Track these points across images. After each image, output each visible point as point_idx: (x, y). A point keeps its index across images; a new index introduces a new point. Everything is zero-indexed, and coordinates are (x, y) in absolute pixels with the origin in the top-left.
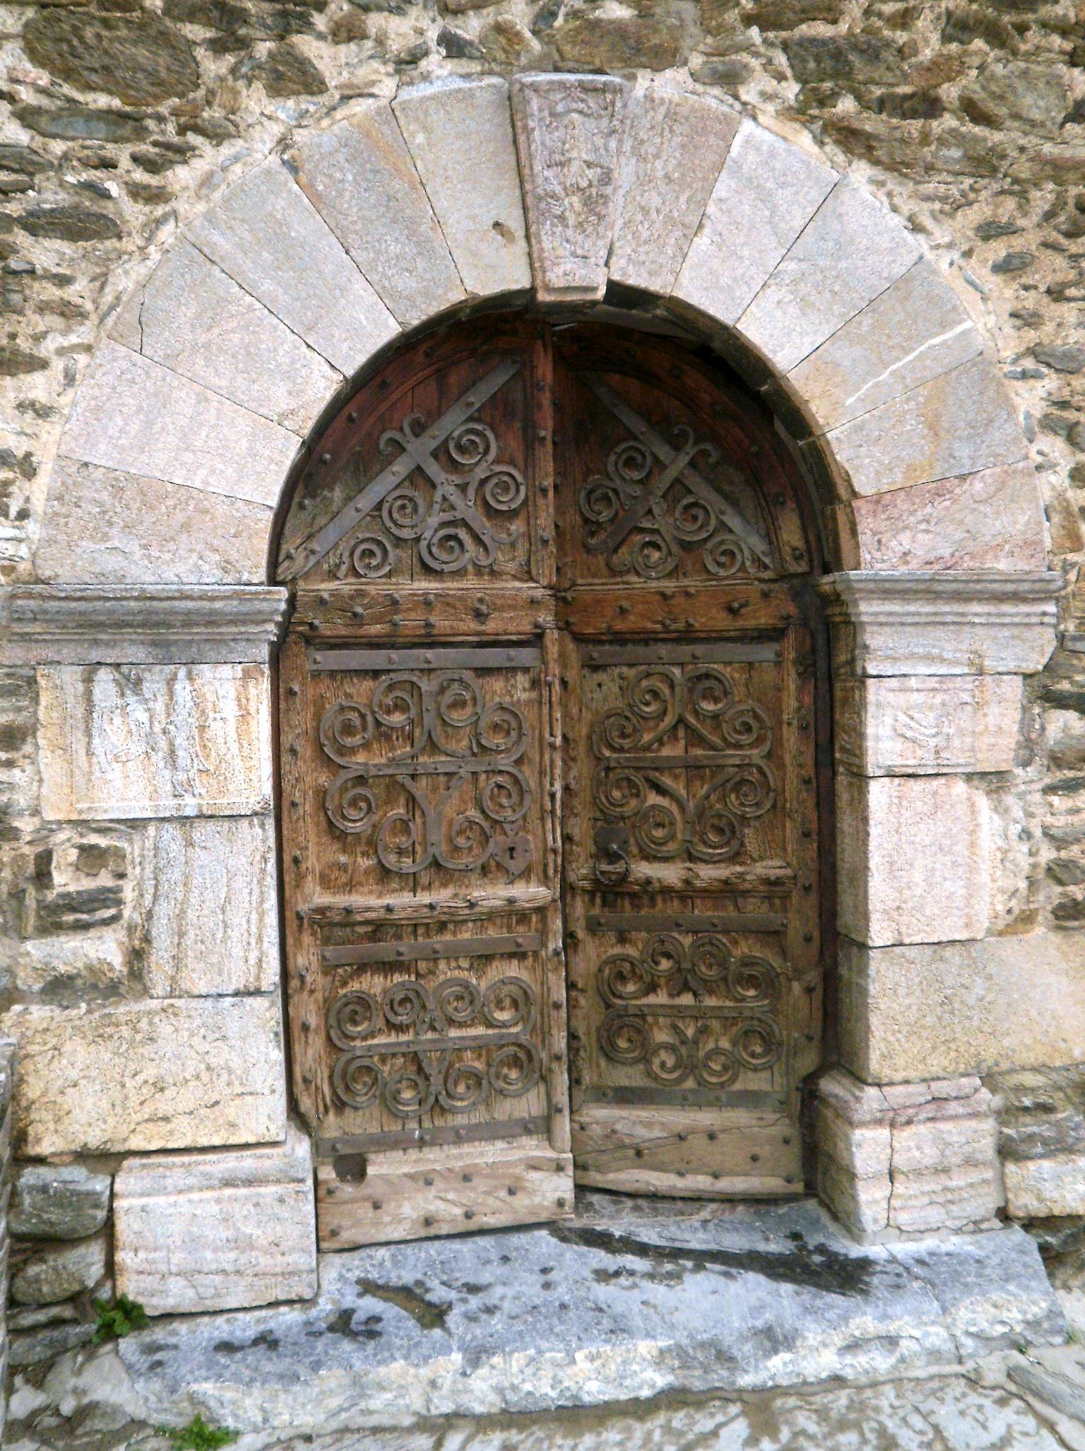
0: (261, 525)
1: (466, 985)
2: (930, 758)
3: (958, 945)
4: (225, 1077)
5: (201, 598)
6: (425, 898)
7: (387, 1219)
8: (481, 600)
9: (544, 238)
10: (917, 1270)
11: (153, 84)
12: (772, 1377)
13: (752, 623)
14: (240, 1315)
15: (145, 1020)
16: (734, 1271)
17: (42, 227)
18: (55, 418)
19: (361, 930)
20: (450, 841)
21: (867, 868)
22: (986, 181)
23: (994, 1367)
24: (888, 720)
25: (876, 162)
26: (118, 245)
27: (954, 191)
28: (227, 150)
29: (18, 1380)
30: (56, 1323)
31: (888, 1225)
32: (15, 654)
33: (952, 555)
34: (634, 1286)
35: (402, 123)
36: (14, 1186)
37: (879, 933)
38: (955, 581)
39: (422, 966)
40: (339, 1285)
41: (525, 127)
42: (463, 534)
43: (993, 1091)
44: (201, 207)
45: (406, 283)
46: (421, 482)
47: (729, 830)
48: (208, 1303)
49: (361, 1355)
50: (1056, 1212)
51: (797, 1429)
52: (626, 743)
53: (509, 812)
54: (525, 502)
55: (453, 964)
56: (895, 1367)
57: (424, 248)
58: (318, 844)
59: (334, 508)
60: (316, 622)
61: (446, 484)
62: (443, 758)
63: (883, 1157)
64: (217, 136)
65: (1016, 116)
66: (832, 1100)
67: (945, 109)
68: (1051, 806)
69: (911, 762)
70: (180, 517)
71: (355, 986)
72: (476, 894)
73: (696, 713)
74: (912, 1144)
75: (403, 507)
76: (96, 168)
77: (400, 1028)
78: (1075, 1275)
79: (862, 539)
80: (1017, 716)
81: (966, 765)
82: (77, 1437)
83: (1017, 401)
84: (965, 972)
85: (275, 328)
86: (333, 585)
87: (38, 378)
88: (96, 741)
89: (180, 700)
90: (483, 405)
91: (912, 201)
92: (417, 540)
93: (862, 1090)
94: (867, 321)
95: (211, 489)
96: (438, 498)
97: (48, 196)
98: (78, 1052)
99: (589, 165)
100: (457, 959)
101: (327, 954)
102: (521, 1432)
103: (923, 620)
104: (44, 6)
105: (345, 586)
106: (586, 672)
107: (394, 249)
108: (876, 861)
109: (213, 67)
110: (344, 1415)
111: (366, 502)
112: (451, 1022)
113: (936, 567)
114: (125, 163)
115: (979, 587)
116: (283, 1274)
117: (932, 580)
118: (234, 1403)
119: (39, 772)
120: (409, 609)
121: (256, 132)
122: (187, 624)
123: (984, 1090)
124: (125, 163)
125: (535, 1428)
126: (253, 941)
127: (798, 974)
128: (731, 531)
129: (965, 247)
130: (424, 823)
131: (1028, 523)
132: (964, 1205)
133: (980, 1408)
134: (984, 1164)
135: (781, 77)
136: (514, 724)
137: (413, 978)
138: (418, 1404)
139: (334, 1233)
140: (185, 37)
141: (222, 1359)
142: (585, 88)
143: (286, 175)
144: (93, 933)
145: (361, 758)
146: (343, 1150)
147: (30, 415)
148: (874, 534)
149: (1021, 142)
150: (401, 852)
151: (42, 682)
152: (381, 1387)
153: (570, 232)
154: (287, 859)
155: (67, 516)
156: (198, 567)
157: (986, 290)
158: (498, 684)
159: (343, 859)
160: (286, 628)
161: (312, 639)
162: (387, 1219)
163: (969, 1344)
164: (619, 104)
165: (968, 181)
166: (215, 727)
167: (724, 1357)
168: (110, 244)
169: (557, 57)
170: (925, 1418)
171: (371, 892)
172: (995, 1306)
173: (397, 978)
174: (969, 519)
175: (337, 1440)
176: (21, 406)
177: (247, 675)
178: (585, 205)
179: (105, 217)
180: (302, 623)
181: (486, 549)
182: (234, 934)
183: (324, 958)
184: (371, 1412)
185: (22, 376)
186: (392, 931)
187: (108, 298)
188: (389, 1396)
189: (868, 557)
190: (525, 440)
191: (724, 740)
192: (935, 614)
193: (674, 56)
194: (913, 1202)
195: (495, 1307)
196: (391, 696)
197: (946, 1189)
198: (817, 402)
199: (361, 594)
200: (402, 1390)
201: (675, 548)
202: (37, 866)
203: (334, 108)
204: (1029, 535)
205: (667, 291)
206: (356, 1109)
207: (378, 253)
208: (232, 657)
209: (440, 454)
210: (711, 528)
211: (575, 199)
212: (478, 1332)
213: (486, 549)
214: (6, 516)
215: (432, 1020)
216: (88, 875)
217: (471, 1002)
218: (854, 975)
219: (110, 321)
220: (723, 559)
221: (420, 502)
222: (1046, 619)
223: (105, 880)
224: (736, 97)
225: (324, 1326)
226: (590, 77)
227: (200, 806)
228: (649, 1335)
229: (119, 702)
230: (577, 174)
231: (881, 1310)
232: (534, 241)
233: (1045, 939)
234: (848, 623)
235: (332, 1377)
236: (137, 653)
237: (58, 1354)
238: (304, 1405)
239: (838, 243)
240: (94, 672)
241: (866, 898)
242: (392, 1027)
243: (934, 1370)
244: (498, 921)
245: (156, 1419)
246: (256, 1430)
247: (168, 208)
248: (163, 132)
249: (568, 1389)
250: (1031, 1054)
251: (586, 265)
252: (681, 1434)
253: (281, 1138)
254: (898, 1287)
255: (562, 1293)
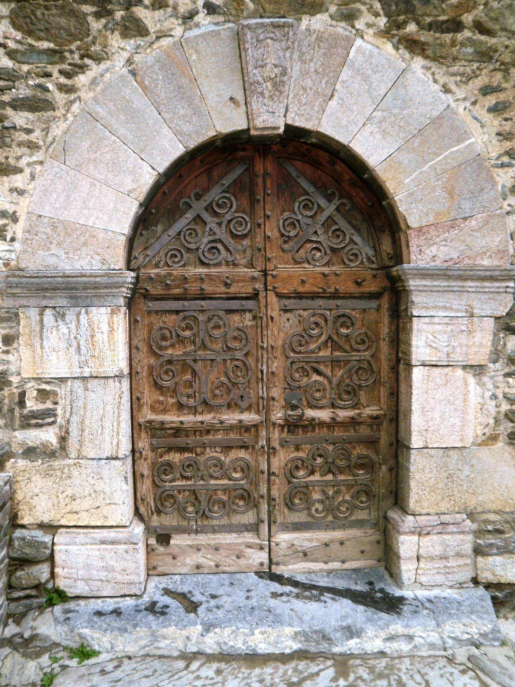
0: (119, 243)
1: (219, 460)
2: (444, 357)
3: (456, 450)
4: (102, 496)
5: (90, 276)
6: (199, 418)
7: (179, 564)
8: (227, 278)
9: (253, 104)
10: (427, 605)
11: (68, 35)
12: (350, 650)
13: (367, 290)
14: (108, 599)
15: (67, 469)
16: (337, 598)
17: (19, 106)
18: (26, 195)
19: (169, 432)
20: (212, 392)
21: (411, 410)
22: (486, 64)
23: (462, 654)
24: (423, 338)
25: (426, 57)
26: (53, 114)
27: (468, 70)
28: (103, 66)
29: (10, 620)
30: (28, 597)
31: (415, 582)
32: (9, 303)
33: (459, 257)
34: (289, 601)
35: (185, 49)
36: (11, 537)
37: (416, 442)
38: (459, 270)
39: (199, 450)
40: (154, 590)
41: (244, 49)
42: (220, 246)
43: (473, 522)
44: (91, 94)
45: (187, 128)
46: (199, 222)
47: (353, 392)
48: (95, 593)
49: (156, 623)
50: (502, 582)
51: (358, 675)
52: (302, 349)
53: (241, 379)
54: (250, 230)
55: (213, 450)
56: (411, 650)
57: (196, 111)
58: (150, 391)
59: (158, 235)
60: (148, 288)
61: (211, 222)
62: (209, 352)
63: (414, 549)
64: (98, 60)
65: (504, 29)
66: (392, 521)
67: (465, 27)
68: (508, 383)
69: (434, 359)
70: (82, 239)
71: (166, 457)
72: (224, 417)
73: (338, 334)
74: (429, 544)
75: (191, 234)
76: (42, 77)
77: (187, 478)
78: (510, 612)
79: (412, 249)
80: (491, 338)
81: (463, 361)
82: (29, 648)
83: (498, 179)
84: (460, 463)
85: (126, 151)
86: (156, 271)
87: (19, 177)
88: (45, 342)
89: (82, 323)
90: (230, 184)
91: (445, 77)
92: (198, 249)
93: (405, 517)
94: (417, 141)
95: (97, 226)
96: (207, 229)
97: (21, 91)
98: (38, 480)
99: (276, 66)
100: (215, 448)
101: (153, 442)
102: (226, 664)
103: (441, 289)
104: (18, 2)
105: (162, 271)
106: (281, 313)
107: (182, 112)
108: (415, 406)
109: (96, 25)
110: (147, 649)
111: (172, 232)
112: (212, 477)
113: (449, 263)
114: (56, 74)
115: (472, 273)
116: (127, 583)
117: (446, 269)
118: (98, 639)
119: (20, 356)
120: (193, 282)
121: (116, 57)
122: (85, 288)
123: (468, 520)
124: (56, 74)
125: (233, 663)
126: (115, 434)
127: (385, 461)
128: (356, 244)
129: (473, 100)
130: (200, 383)
131: (500, 241)
132: (455, 575)
133: (452, 674)
134: (466, 556)
135: (377, 15)
136: (244, 337)
137: (194, 455)
138: (181, 647)
139: (154, 568)
140: (83, 12)
141: (96, 619)
142: (275, 26)
143: (130, 77)
144: (44, 429)
145: (170, 351)
146: (160, 531)
147: (15, 194)
148: (418, 247)
149: (507, 43)
150: (189, 396)
151: (21, 315)
152: (164, 638)
153: (266, 101)
154: (134, 397)
155: (32, 240)
156: (91, 262)
157: (483, 122)
158: (236, 318)
159: (161, 398)
160: (134, 291)
161: (147, 296)
162: (179, 564)
163: (450, 642)
164: (291, 33)
165: (476, 65)
166: (98, 336)
167: (326, 638)
168: (50, 113)
169: (262, 11)
170: (422, 676)
171: (174, 414)
172: (464, 625)
173: (186, 455)
174: (468, 239)
175: (144, 660)
176: (11, 190)
177: (113, 312)
178: (273, 86)
179: (47, 100)
180: (142, 288)
181: (231, 253)
182: (106, 431)
183: (152, 444)
184: (159, 648)
185: (11, 176)
186: (184, 433)
187: (50, 139)
188: (167, 642)
189: (415, 258)
190: (250, 201)
191: (351, 347)
192: (448, 286)
193: (322, 7)
194: (429, 572)
195: (222, 606)
196: (184, 322)
197: (446, 567)
198: (390, 181)
199: (170, 275)
200: (174, 640)
201: (328, 252)
202: (19, 398)
203: (153, 43)
204: (500, 248)
205: (315, 128)
206: (166, 514)
207: (175, 114)
208: (105, 303)
209: (209, 208)
210: (347, 242)
211: (268, 84)
212: (211, 617)
213: (231, 253)
214: (5, 240)
215: (202, 476)
216: (41, 402)
217: (221, 468)
218: (404, 461)
219: (51, 150)
220: (352, 258)
221: (199, 232)
222: (508, 290)
223: (49, 405)
224: (353, 27)
225: (143, 607)
226: (277, 20)
227: (91, 372)
228: (290, 625)
229: (55, 324)
230: (270, 71)
231: (406, 622)
232: (249, 106)
233: (503, 448)
234: (405, 290)
235: (142, 631)
236: (63, 302)
237: (28, 611)
238: (129, 642)
239: (404, 101)
240: (44, 310)
241: (410, 424)
242: (183, 477)
243: (432, 653)
244: (235, 430)
245: (64, 643)
246: (108, 652)
247: (76, 95)
248: (73, 59)
249: (251, 646)
250: (494, 505)
251: (273, 117)
252: (301, 672)
253: (128, 524)
254: (416, 612)
255: (254, 602)
